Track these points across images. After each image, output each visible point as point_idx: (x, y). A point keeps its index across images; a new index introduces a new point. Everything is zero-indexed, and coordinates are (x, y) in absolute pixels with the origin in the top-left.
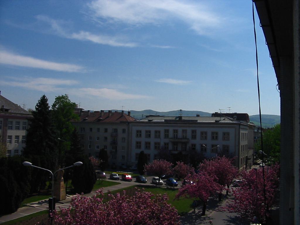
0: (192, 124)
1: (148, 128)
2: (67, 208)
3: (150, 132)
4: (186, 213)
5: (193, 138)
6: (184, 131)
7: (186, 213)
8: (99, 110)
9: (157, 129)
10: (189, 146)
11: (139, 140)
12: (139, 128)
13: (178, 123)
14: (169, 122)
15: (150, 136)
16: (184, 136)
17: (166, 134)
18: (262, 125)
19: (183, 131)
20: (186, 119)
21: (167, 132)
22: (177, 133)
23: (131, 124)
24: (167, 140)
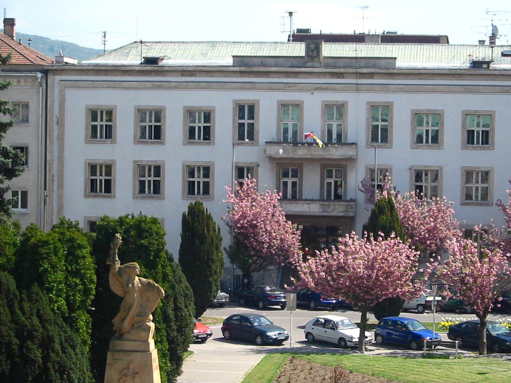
0: (371, 75)
1: (150, 99)
2: (19, 313)
3: (158, 115)
4: (505, 206)
5: (374, 139)
6: (336, 110)
7: (505, 206)
8: (70, 42)
9: (200, 99)
10: (355, 180)
11: (101, 152)
12: (103, 98)
13: (303, 70)
14: (256, 69)
15: (157, 133)
16: (286, 131)
17: (241, 126)
18: (48, 159)
19: (284, 106)
20: (503, 82)
21: (197, 121)
22: (251, 117)
23: (55, 80)
24: (247, 154)
